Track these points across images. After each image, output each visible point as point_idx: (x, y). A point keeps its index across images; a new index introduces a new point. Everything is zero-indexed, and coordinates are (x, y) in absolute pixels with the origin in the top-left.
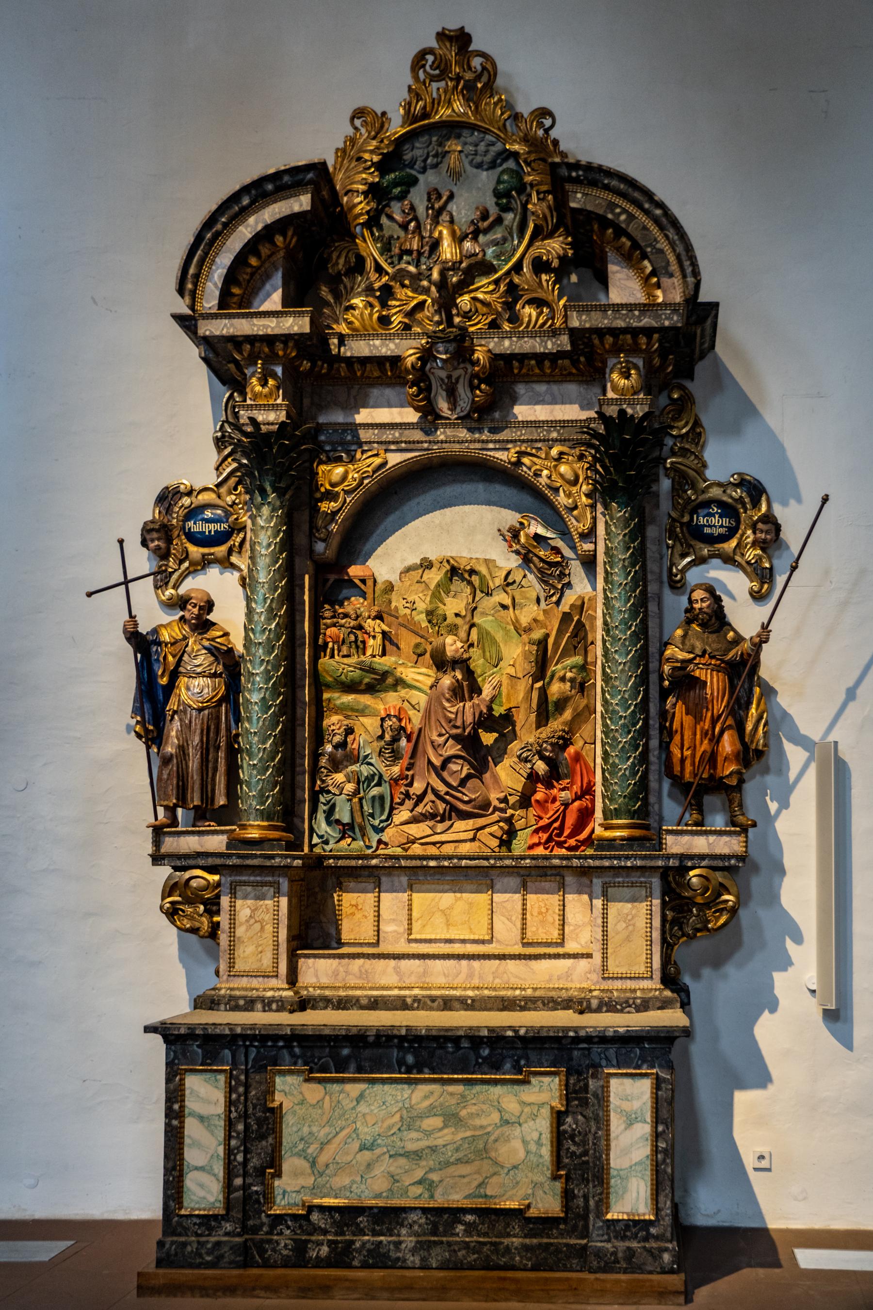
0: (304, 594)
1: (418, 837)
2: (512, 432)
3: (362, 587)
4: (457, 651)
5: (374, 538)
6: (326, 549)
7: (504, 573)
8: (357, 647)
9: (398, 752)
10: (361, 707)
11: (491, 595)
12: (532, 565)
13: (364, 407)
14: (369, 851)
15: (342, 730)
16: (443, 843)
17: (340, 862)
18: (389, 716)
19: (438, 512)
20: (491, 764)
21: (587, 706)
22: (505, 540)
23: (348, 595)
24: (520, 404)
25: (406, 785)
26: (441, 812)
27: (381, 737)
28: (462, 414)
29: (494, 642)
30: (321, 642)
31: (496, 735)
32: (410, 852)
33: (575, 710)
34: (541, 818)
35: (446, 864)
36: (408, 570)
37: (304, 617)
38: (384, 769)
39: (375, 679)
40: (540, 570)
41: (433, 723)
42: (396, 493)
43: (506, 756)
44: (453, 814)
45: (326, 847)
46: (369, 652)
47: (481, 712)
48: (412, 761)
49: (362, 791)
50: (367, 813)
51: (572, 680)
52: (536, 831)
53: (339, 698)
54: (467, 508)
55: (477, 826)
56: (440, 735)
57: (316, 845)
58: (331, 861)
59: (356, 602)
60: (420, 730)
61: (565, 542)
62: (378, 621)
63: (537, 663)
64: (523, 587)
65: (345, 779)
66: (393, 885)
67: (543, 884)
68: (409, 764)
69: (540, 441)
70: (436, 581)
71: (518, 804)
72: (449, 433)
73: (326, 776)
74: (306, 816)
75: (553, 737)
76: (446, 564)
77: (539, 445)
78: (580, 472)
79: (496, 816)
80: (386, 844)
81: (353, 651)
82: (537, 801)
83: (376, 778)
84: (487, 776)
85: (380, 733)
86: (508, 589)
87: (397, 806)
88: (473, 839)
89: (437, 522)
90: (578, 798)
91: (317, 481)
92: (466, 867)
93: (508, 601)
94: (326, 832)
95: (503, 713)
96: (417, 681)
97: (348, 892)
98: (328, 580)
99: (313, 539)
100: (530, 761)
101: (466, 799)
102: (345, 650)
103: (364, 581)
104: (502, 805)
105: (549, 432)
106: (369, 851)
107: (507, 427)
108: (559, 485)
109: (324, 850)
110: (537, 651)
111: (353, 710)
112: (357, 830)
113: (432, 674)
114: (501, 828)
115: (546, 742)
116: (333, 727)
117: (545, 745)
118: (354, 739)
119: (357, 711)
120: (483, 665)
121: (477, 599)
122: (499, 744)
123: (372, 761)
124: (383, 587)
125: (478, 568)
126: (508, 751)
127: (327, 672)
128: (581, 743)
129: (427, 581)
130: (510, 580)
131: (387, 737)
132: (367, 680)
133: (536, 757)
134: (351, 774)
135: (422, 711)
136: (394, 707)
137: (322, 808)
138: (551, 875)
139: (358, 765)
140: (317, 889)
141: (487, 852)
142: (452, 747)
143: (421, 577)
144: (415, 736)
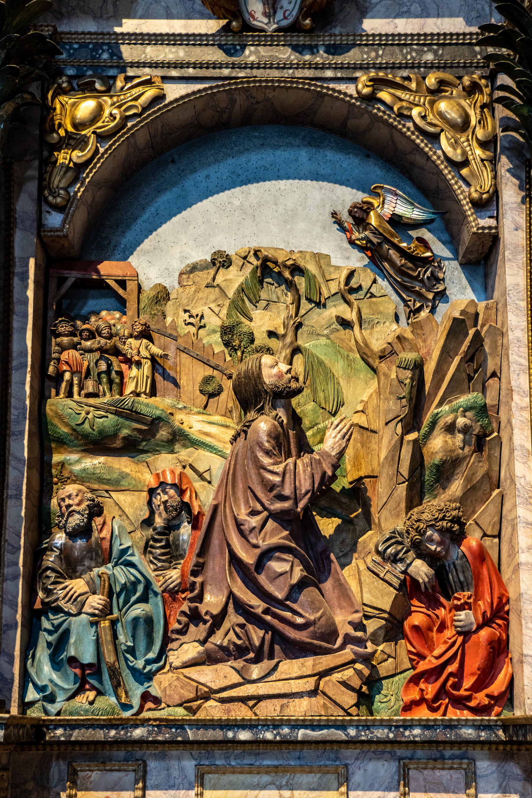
0: (26, 287)
1: (215, 687)
2: (362, 53)
3: (121, 291)
4: (280, 376)
5: (137, 227)
6: (64, 221)
7: (344, 274)
8: (111, 382)
9: (177, 546)
10: (115, 476)
11: (324, 306)
12: (386, 264)
13: (128, 17)
14: (127, 714)
15: (84, 506)
16: (259, 698)
17: (76, 733)
18: (162, 484)
19: (238, 189)
20: (335, 565)
21: (487, 475)
22: (343, 229)
23: (96, 309)
24: (372, 17)
25: (191, 600)
26: (257, 643)
27: (148, 522)
28: (285, 23)
29: (329, 376)
30: (51, 369)
31: (337, 521)
32: (201, 715)
33: (468, 480)
34: (422, 657)
35: (269, 736)
36: (194, 268)
37: (26, 323)
38: (153, 574)
39: (139, 431)
40: (400, 271)
41: (240, 494)
42: (173, 161)
43: (355, 555)
44: (277, 647)
45: (49, 707)
46: (130, 388)
47: (324, 473)
48: (201, 560)
49: (115, 610)
50: (123, 647)
51: (466, 430)
52: (415, 680)
53: (78, 461)
54: (283, 184)
55: (320, 668)
56: (253, 513)
57: (32, 704)
58: (59, 732)
59: (108, 318)
60: (215, 509)
61: (434, 235)
62: (145, 341)
63: (410, 400)
64: (373, 296)
65: (86, 589)
66: (169, 775)
67: (438, 773)
68: (197, 565)
69: (406, 67)
70: (236, 286)
71: (382, 633)
72: (263, 53)
73: (55, 583)
74: (17, 653)
75: (443, 519)
76: (252, 259)
77: (405, 73)
78: (471, 113)
79: (348, 653)
80: (157, 701)
81: (104, 387)
82: (416, 628)
83: (140, 588)
84: (328, 586)
85: (147, 515)
86: (352, 298)
87: (174, 636)
88: (314, 693)
89: (237, 203)
90: (486, 622)
91: (52, 120)
92: (303, 742)
93: (351, 315)
94: (51, 681)
95: (347, 486)
96: (207, 434)
97: (87, 789)
98: (66, 279)
99: (45, 208)
100: (402, 560)
101: (299, 620)
102: (90, 386)
103: (122, 284)
104: (359, 634)
105: (421, 53)
106: (127, 714)
107: (354, 45)
108: (438, 130)
109: (46, 712)
110: (412, 379)
111: (100, 480)
112: (106, 677)
113: (232, 425)
114: (359, 673)
115: (432, 526)
116: (68, 502)
117: (429, 533)
118: (104, 523)
119: (108, 482)
120: (314, 411)
121: (302, 312)
122: (344, 535)
123: (135, 559)
124: (153, 293)
125: (302, 263)
126: (359, 547)
127: (60, 417)
128: (478, 534)
129: (223, 285)
130: (354, 283)
131: (159, 522)
132: (125, 432)
133: (411, 554)
134: (97, 581)
135: (216, 483)
136: (172, 472)
137: (44, 638)
138: (451, 758)
139: (110, 565)
140: (30, 785)
141: (338, 714)
142: (273, 533)
143: (214, 279)
144: (205, 521)
